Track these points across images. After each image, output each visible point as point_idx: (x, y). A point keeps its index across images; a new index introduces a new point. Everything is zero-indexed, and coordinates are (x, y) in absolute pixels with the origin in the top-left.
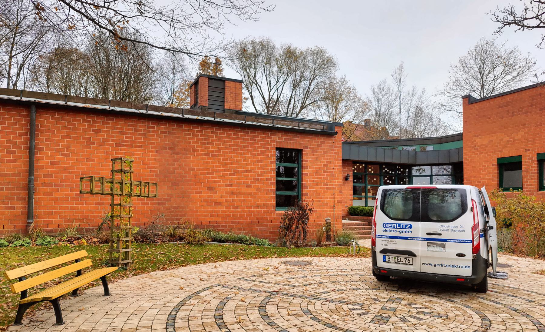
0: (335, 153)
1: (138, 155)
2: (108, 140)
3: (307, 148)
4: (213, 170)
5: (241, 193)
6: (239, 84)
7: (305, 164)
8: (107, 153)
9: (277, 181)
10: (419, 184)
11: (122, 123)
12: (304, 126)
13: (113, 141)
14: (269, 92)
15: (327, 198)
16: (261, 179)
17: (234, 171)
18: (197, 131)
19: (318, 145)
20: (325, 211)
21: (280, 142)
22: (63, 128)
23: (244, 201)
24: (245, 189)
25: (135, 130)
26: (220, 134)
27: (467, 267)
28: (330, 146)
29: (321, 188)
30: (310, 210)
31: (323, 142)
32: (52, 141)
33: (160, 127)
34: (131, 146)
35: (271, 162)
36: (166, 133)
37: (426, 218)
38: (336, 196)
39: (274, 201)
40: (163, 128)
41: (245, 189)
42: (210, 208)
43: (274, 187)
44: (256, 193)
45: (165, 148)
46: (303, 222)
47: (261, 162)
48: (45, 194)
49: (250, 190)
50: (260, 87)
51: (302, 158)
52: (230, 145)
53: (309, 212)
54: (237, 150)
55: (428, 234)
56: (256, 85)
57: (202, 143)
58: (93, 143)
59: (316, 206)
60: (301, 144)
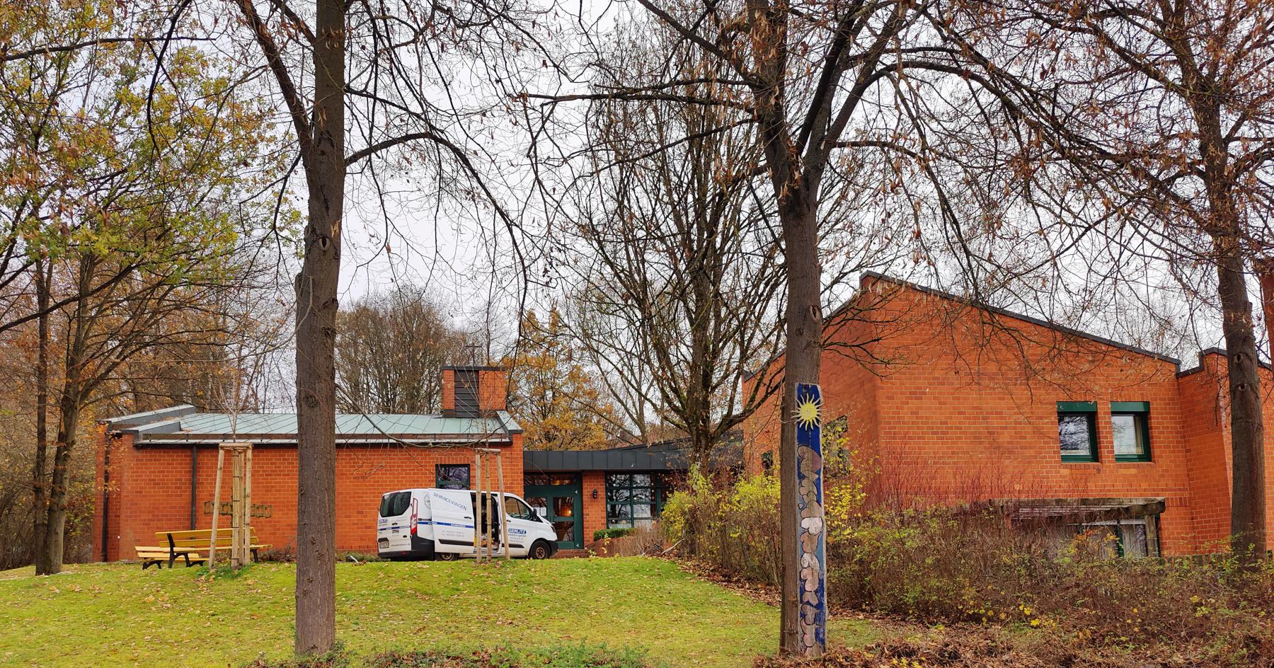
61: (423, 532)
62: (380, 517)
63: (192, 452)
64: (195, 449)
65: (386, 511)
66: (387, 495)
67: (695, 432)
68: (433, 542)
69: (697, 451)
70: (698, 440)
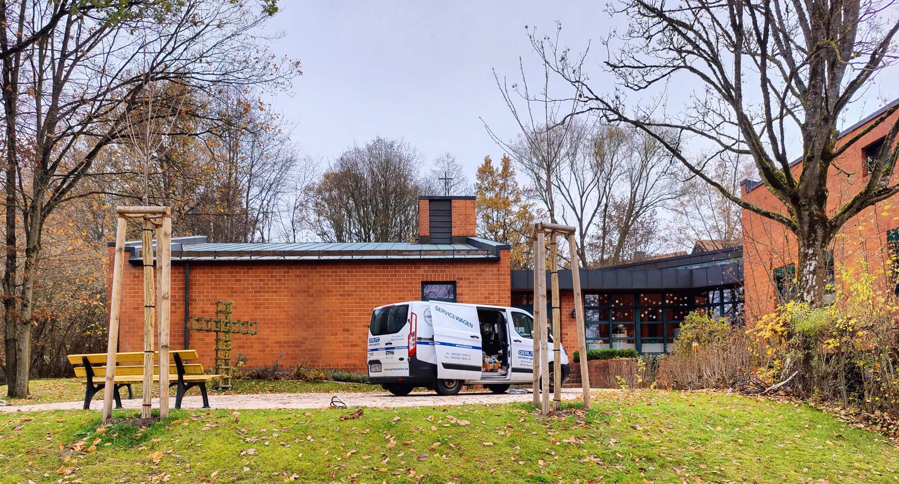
0: (499, 282)
1: (275, 300)
3: (462, 279)
4: (348, 311)
6: (470, 201)
8: (248, 300)
11: (369, 270)
13: (252, 288)
14: (581, 197)
21: (427, 275)
22: (211, 280)
26: (356, 272)
27: (406, 369)
28: (493, 275)
32: (203, 292)
34: (268, 292)
40: (298, 272)
42: (346, 351)
45: (299, 292)
48: (199, 340)
50: (568, 191)
52: (367, 283)
55: (387, 344)
57: (336, 284)
58: (236, 292)
60: (454, 275)
61: (424, 354)
62: (371, 336)
63: (185, 269)
64: (187, 266)
65: (376, 329)
66: (378, 309)
67: (806, 219)
68: (434, 367)
69: (809, 246)
70: (812, 229)
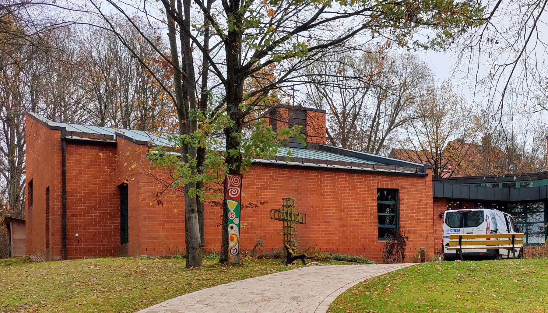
0: (427, 192)
2: (251, 185)
3: (403, 188)
4: (328, 207)
5: (350, 226)
7: (401, 201)
9: (379, 216)
10: (466, 209)
12: (400, 169)
15: (421, 230)
16: (366, 214)
17: (344, 208)
18: (315, 176)
19: (412, 185)
20: (420, 241)
23: (353, 232)
24: (353, 222)
25: (270, 176)
28: (422, 186)
29: (416, 221)
30: (407, 238)
31: (417, 183)
33: (288, 174)
35: (373, 200)
36: (292, 178)
37: (466, 226)
38: (428, 228)
39: (376, 232)
41: (353, 222)
43: (376, 220)
44: (361, 226)
46: (401, 247)
47: (365, 200)
49: (357, 223)
51: (398, 196)
53: (406, 239)
54: (346, 190)
55: (467, 233)
56: (326, 98)
57: (319, 185)
59: (411, 236)
